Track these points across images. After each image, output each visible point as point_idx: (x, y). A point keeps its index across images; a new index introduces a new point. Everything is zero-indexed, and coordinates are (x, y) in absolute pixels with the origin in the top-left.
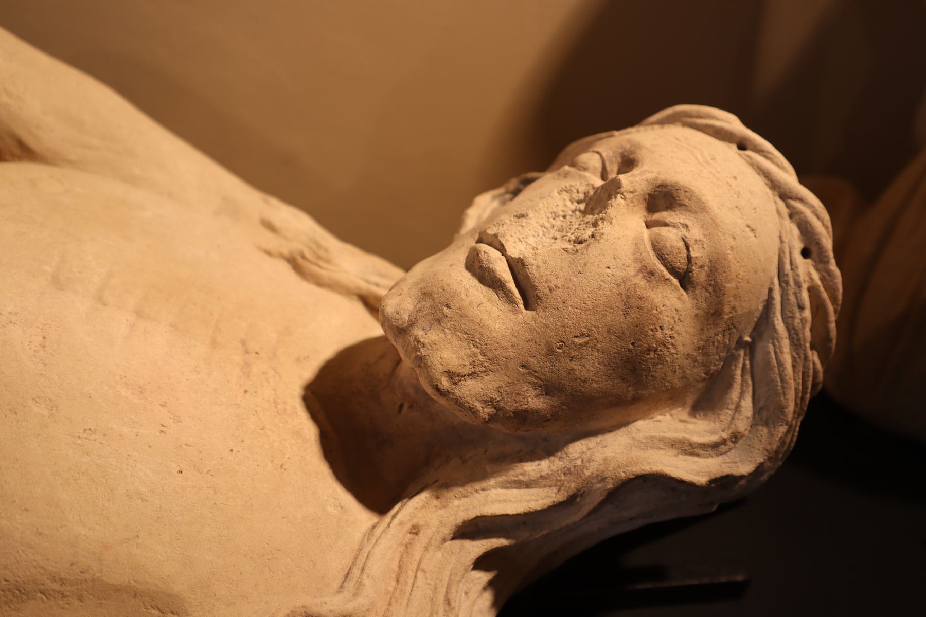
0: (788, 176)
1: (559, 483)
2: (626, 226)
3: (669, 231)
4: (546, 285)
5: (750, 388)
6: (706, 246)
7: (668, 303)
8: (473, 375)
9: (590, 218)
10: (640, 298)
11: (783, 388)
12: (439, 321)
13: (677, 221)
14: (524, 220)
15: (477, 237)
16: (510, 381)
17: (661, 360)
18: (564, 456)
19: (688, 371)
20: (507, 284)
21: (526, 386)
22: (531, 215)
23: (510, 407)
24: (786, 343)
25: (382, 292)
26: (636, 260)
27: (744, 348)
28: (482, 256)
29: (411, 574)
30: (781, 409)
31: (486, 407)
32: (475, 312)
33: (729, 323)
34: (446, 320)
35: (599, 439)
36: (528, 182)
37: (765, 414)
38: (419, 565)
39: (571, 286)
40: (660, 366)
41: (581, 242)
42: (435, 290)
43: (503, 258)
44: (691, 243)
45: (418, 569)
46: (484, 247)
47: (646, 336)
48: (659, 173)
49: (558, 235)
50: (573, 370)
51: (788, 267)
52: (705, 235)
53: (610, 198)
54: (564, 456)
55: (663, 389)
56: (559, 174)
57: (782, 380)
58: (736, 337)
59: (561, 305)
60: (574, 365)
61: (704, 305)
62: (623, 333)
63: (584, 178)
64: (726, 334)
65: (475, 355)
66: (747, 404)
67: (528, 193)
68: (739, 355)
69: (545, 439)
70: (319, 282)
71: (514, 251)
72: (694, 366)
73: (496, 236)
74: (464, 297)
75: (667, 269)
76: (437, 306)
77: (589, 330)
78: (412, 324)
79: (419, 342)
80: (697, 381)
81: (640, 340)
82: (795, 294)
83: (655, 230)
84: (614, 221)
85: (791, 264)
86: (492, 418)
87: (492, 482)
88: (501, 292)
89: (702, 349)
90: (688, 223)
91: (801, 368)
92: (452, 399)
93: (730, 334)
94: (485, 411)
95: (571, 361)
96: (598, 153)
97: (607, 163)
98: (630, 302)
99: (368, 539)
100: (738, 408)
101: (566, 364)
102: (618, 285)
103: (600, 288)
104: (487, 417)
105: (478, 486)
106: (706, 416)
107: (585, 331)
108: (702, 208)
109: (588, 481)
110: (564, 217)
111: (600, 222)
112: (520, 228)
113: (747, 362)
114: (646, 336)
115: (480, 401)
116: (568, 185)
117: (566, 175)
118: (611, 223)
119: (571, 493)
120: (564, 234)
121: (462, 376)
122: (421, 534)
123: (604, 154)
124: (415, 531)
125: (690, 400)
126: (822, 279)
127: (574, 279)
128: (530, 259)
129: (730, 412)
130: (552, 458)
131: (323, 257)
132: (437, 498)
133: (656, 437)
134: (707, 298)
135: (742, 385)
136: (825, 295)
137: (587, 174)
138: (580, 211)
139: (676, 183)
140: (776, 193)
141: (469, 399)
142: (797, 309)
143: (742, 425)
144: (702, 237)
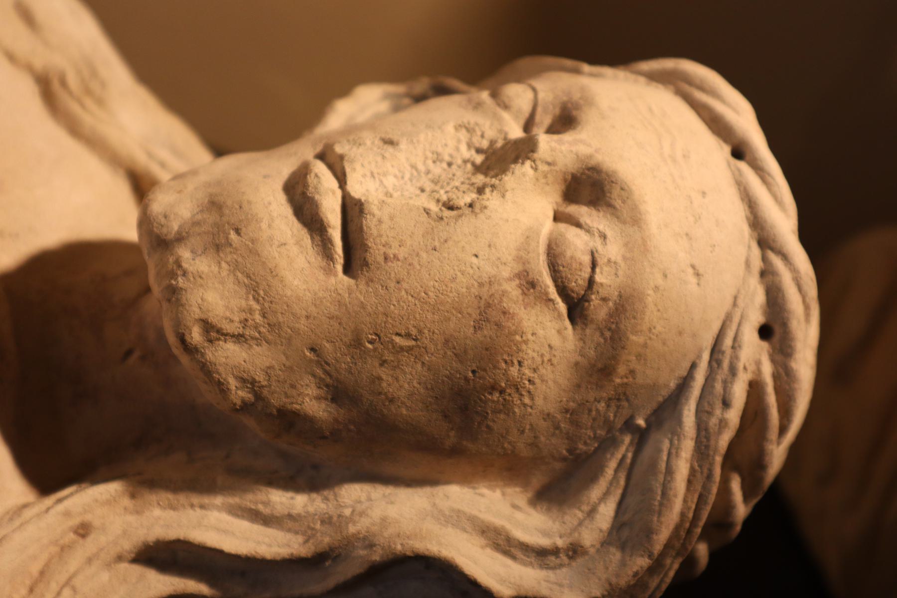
0: (784, 220)
1: (310, 532)
2: (525, 208)
3: (577, 235)
4: (383, 250)
5: (619, 492)
6: (620, 273)
7: (541, 332)
8: (239, 338)
9: (480, 179)
10: (504, 313)
11: (661, 504)
12: (218, 248)
13: (595, 225)
14: (390, 149)
15: (319, 149)
16: (288, 364)
17: (506, 408)
18: (331, 497)
19: (542, 439)
20: (330, 231)
21: (308, 379)
22: (403, 146)
23: (276, 401)
24: (688, 447)
25: (164, 176)
26: (518, 259)
27: (633, 433)
28: (311, 179)
29: (54, 587)
30: (649, 532)
31: (241, 388)
32: (272, 253)
33: (620, 390)
34: (229, 250)
35: (389, 490)
36: (442, 91)
37: (625, 533)
38: (70, 579)
39: (416, 263)
40: (502, 416)
41: (451, 208)
42: (229, 203)
43: (339, 193)
44: (601, 261)
45: (68, 583)
46: (320, 168)
47: (495, 367)
48: (597, 151)
49: (429, 186)
50: (380, 379)
51: (728, 342)
52: (624, 258)
53: (515, 161)
54: (331, 497)
55: (500, 450)
56: (470, 101)
57: (664, 494)
58: (626, 413)
59: (392, 285)
60: (384, 373)
61: (592, 353)
62: (465, 351)
63: (499, 119)
64: (613, 404)
65: (251, 311)
66: (607, 512)
67: (420, 112)
68: (622, 442)
69: (315, 467)
70: (74, 129)
71: (357, 188)
72: (553, 435)
73: (342, 157)
74: (264, 226)
75: (557, 286)
76: (222, 226)
77: (420, 332)
78: (180, 239)
79: (180, 266)
80: (553, 457)
81: (485, 370)
82: (725, 382)
83: (562, 227)
84: (508, 195)
85: (735, 339)
86: (246, 407)
87: (219, 500)
88: (317, 238)
89: (572, 414)
90: (609, 233)
91: (699, 488)
92: (199, 362)
93: (618, 407)
94: (239, 394)
95: (381, 365)
96: (534, 90)
97: (539, 110)
98: (489, 312)
99: (11, 519)
100: (592, 512)
101: (371, 366)
102: (481, 285)
103: (454, 279)
104: (239, 402)
105: (196, 499)
106: (549, 510)
107: (414, 332)
108: (635, 220)
109: (349, 543)
110: (450, 164)
111: (488, 190)
112: (379, 159)
113: (630, 455)
114: (495, 367)
115: (236, 377)
116: (472, 121)
117: (478, 106)
118: (503, 196)
119: (321, 548)
120: (437, 188)
121: (223, 335)
122: (89, 539)
123: (541, 95)
124: (83, 530)
125: (538, 480)
126: (776, 377)
127: (424, 255)
128: (373, 207)
129: (580, 515)
130: (314, 495)
131: (94, 90)
132: (133, 496)
133: (464, 513)
134: (598, 344)
135: (611, 483)
136: (771, 399)
137: (505, 115)
138: (473, 164)
139: (614, 172)
140: (756, 234)
141: (221, 369)
142: (718, 405)
143: (589, 537)
144: (619, 259)
